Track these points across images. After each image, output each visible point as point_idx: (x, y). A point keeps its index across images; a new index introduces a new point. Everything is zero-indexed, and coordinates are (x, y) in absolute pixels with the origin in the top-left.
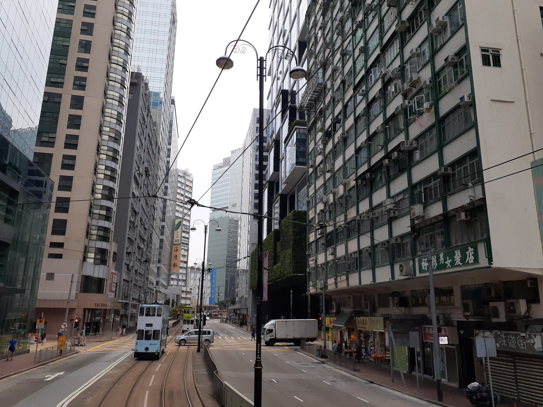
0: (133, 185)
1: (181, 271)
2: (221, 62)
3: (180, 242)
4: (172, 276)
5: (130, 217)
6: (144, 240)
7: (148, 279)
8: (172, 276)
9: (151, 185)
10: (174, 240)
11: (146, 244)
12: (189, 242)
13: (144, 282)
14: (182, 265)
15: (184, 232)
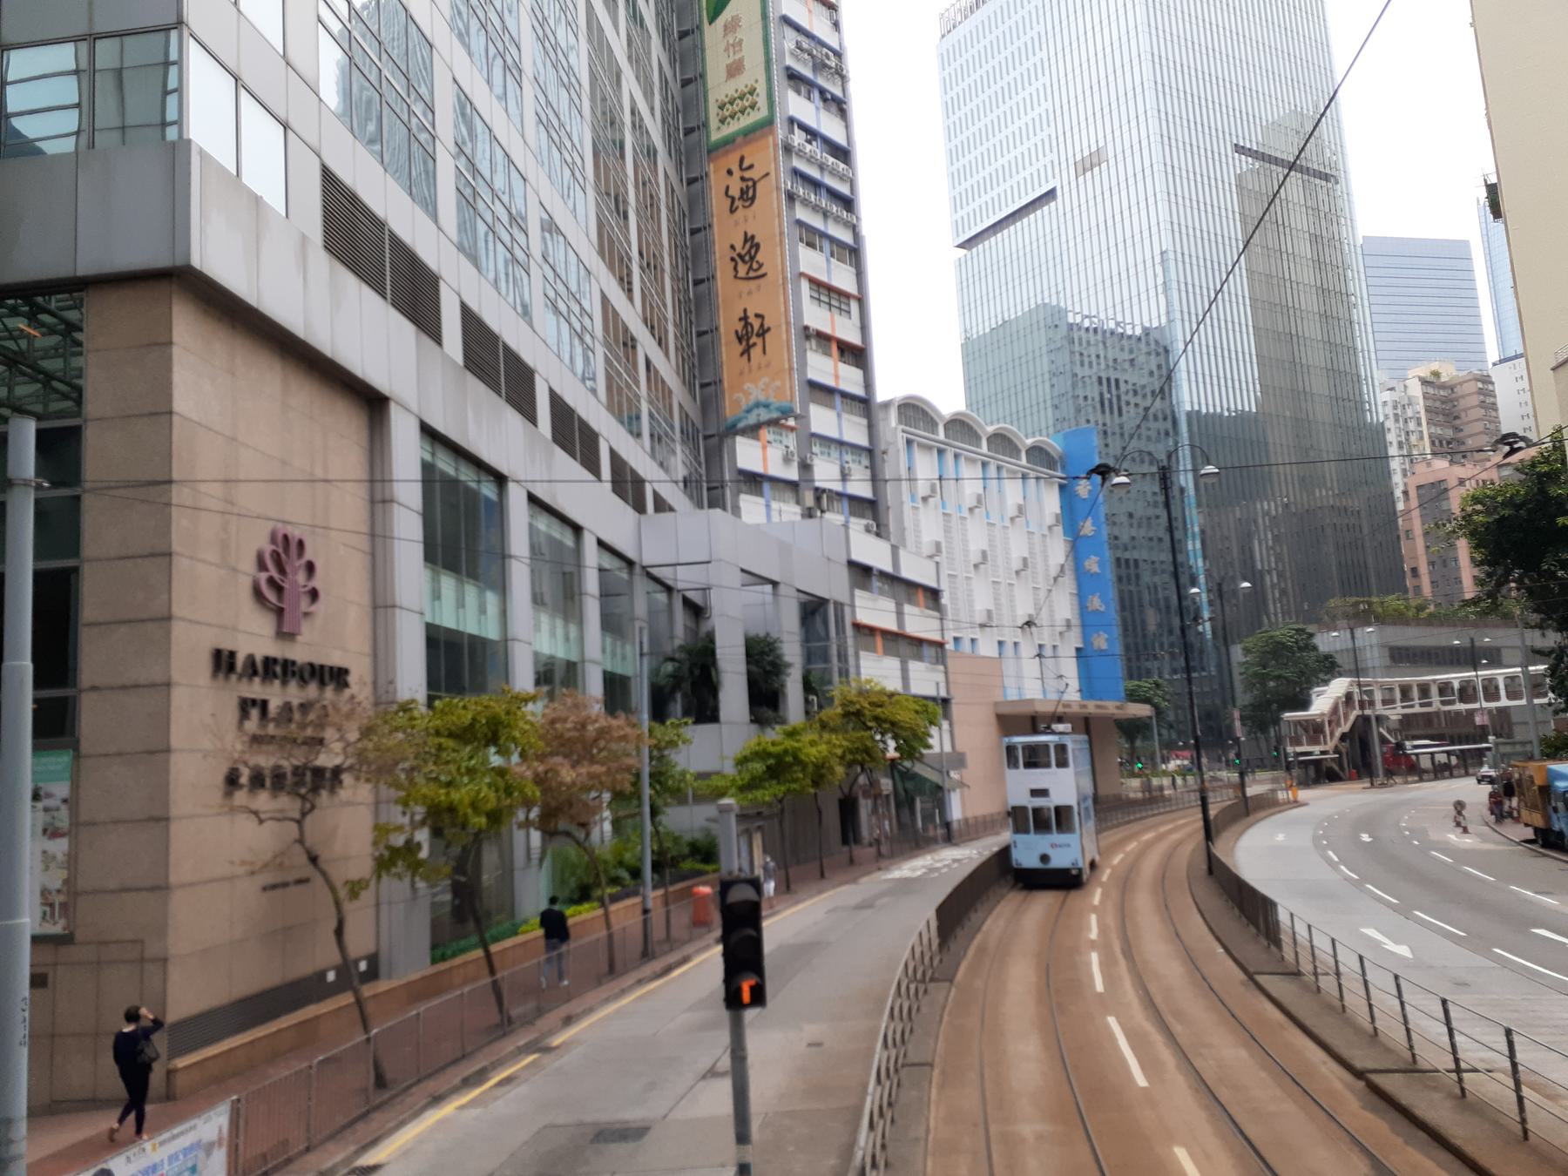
2: (910, 413)
3: (762, 101)
4: (748, 454)
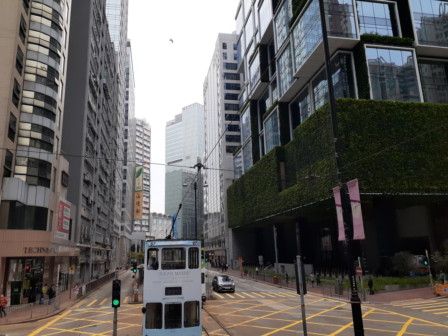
0: (89, 97)
1: (144, 217)
3: (141, 188)
4: (136, 223)
5: (87, 134)
6: (106, 174)
7: (113, 221)
8: (136, 223)
9: (111, 113)
10: (136, 187)
11: (109, 180)
12: (150, 189)
13: (109, 225)
14: (144, 211)
15: (145, 179)
